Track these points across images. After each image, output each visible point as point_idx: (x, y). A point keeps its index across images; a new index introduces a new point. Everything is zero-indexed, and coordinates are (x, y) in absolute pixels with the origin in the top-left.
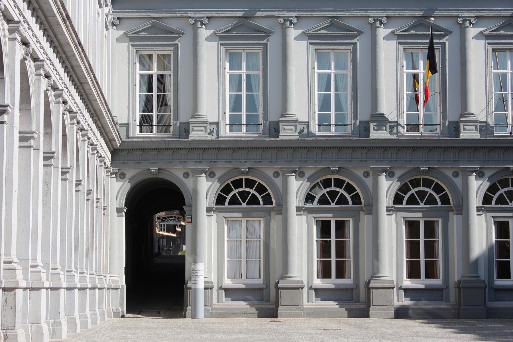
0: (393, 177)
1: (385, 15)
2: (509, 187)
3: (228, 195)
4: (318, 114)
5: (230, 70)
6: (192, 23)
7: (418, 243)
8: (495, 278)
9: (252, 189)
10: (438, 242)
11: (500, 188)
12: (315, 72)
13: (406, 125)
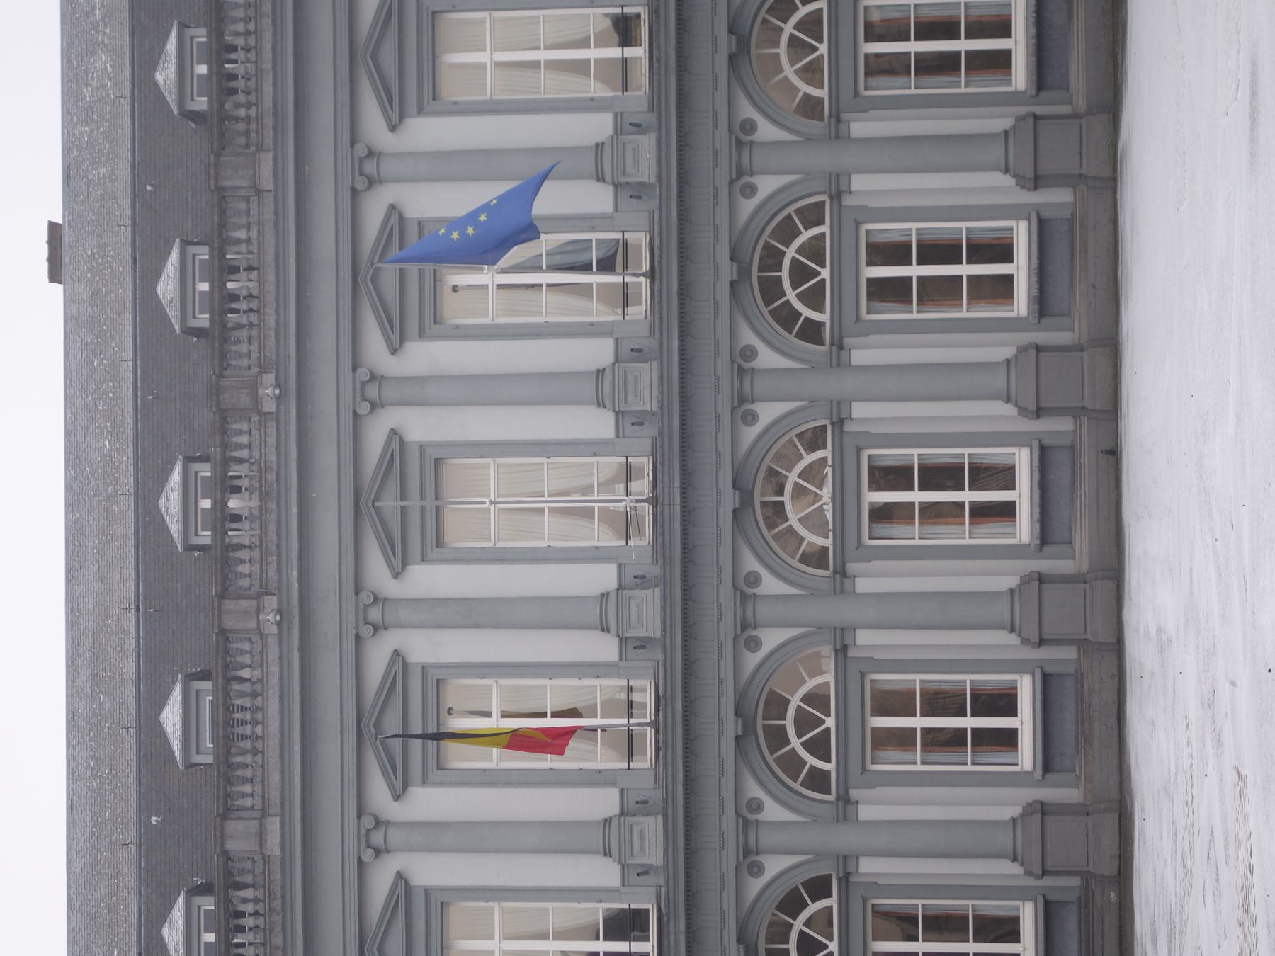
0: (755, 348)
1: (356, 820)
2: (780, 277)
3: (806, 763)
4: (602, 717)
5: (485, 50)
6: (373, 825)
8: (1010, 88)
9: (785, 253)
10: (923, 457)
12: (497, 768)
13: (625, 93)
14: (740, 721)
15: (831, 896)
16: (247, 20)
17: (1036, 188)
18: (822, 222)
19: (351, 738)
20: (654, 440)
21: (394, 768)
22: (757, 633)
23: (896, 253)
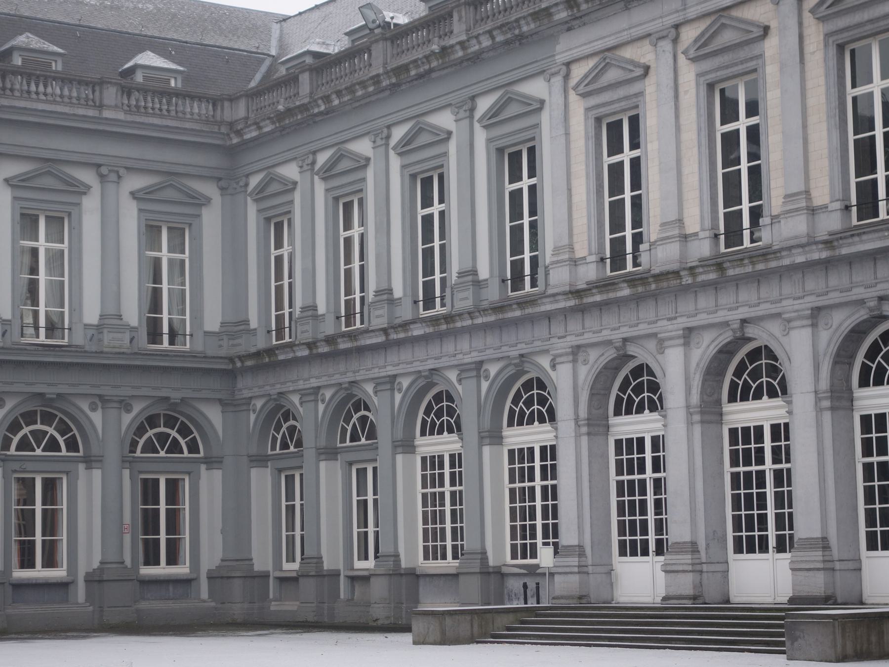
7: (157, 511)
11: (148, 429)
14: (55, 396)
15: (189, 453)
16: (78, 99)
17: (86, 581)
18: (190, 452)
19: (165, 168)
20: (83, 347)
21: (23, 180)
22: (100, 411)
23: (173, 495)
